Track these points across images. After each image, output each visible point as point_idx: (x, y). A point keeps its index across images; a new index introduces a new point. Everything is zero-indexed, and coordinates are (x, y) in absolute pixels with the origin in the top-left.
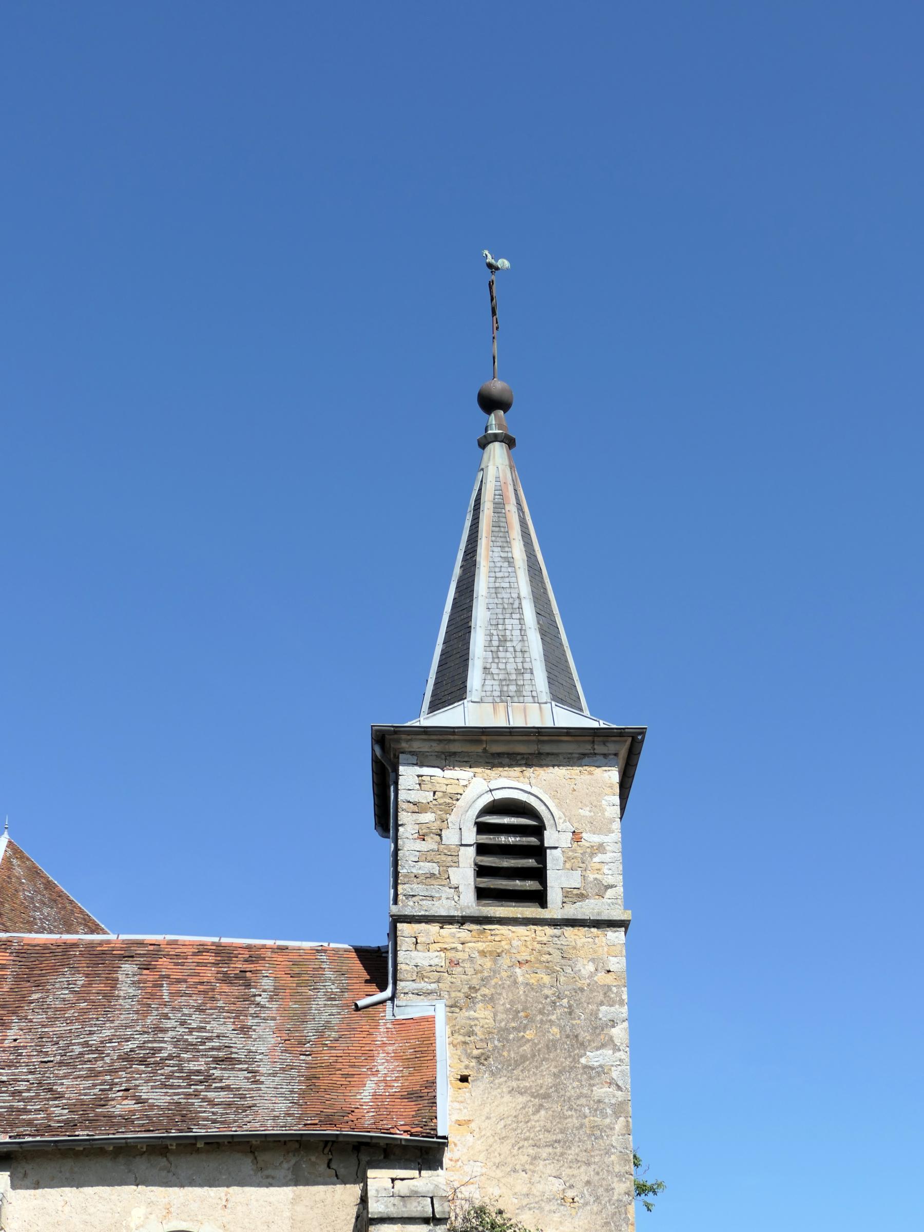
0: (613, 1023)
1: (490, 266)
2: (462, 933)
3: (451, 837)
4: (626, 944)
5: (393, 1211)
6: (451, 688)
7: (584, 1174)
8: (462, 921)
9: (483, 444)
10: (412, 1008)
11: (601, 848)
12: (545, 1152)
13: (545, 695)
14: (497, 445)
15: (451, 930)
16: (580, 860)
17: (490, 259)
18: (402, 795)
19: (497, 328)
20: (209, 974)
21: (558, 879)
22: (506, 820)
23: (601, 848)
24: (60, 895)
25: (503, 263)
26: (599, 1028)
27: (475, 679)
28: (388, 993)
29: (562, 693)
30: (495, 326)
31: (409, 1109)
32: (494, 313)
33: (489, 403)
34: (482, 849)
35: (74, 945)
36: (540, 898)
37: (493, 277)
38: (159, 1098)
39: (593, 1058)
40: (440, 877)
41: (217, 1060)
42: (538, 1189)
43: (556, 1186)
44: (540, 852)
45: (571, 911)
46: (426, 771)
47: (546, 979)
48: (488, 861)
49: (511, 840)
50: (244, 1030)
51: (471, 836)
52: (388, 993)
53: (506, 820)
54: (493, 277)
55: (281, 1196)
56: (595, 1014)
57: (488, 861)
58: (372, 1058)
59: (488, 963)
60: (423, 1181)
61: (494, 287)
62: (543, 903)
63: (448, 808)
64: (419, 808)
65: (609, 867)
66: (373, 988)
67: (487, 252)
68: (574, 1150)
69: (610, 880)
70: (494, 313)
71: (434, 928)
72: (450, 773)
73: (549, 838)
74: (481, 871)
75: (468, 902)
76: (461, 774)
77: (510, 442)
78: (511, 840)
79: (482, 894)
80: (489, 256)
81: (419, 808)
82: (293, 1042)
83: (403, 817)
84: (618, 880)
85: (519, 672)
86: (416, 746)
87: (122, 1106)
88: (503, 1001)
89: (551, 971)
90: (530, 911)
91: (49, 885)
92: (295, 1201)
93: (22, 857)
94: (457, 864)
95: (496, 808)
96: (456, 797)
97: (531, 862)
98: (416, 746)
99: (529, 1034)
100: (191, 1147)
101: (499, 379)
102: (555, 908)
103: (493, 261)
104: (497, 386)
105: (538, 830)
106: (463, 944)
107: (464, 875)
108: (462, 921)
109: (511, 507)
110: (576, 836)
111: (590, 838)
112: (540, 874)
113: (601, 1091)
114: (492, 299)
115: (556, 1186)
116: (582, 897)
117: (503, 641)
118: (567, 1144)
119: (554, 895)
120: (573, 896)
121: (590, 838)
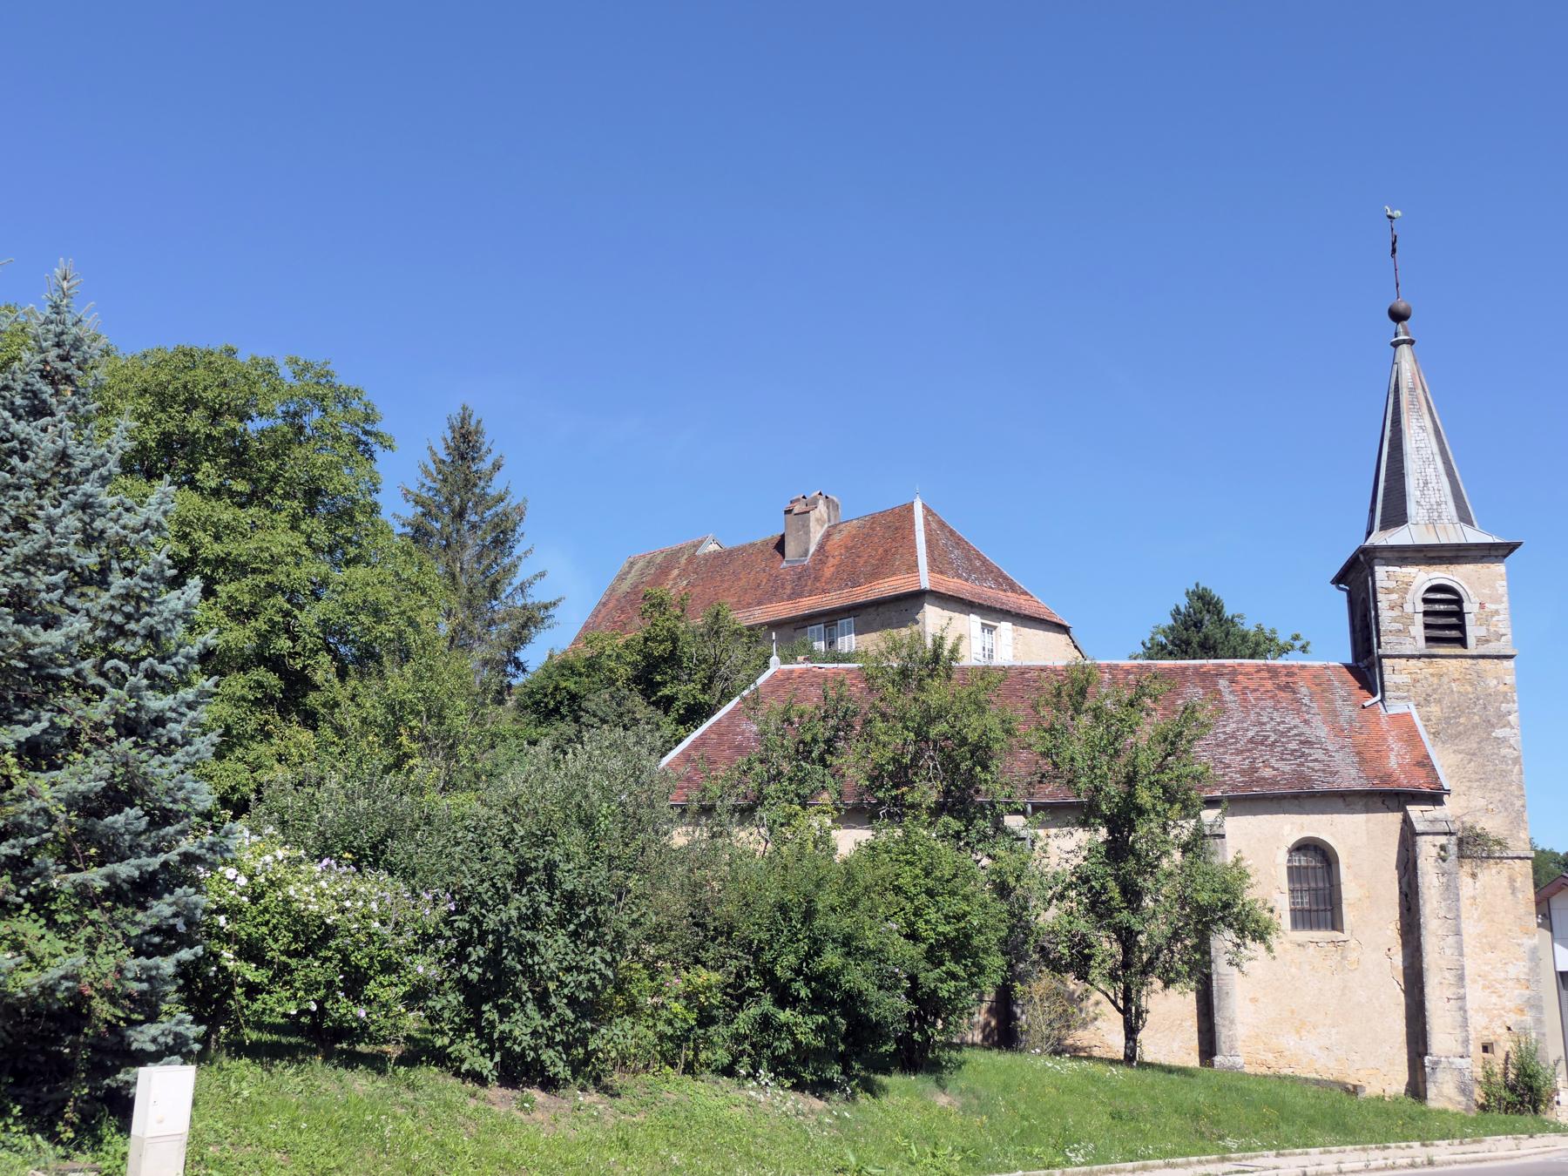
0: (1509, 713)
2: (1420, 663)
3: (1408, 608)
4: (1516, 668)
5: (1428, 829)
6: (1395, 514)
7: (1498, 796)
8: (1419, 657)
9: (1396, 345)
10: (1396, 708)
11: (1497, 612)
12: (1475, 785)
13: (1456, 519)
14: (1405, 346)
15: (1412, 662)
16: (1485, 620)
18: (1378, 584)
20: (1269, 685)
21: (1473, 631)
22: (1439, 596)
23: (1497, 612)
24: (960, 539)
25: (1397, 213)
26: (1502, 717)
27: (1412, 508)
28: (1379, 697)
29: (1465, 517)
31: (1421, 772)
32: (1394, 251)
33: (1398, 316)
34: (1426, 614)
35: (1186, 668)
36: (1462, 642)
38: (1286, 767)
39: (1499, 733)
40: (1404, 632)
41: (1302, 742)
42: (1472, 804)
43: (1483, 802)
44: (1460, 614)
45: (1482, 650)
46: (1391, 568)
47: (1470, 689)
48: (1431, 620)
49: (1442, 607)
50: (1306, 722)
51: (1421, 607)
52: (1379, 697)
53: (1439, 596)
55: (1361, 818)
56: (1499, 708)
57: (1431, 620)
58: (1385, 740)
59: (1435, 680)
60: (1435, 812)
62: (1464, 645)
63: (1406, 591)
64: (1389, 591)
65: (1502, 623)
66: (1365, 693)
68: (1491, 784)
69: (1503, 631)
70: (1394, 251)
71: (1404, 661)
72: (1404, 570)
73: (1467, 607)
74: (1427, 626)
75: (1421, 646)
76: (1411, 570)
77: (1411, 342)
78: (1442, 607)
79: (1428, 639)
81: (1389, 591)
82: (1338, 732)
83: (1380, 596)
84: (1508, 631)
85: (1438, 504)
86: (1385, 554)
87: (1267, 773)
88: (1446, 702)
89: (1472, 685)
90: (1459, 651)
91: (952, 532)
92: (1368, 821)
93: (933, 515)
94: (1413, 624)
95: (1432, 589)
96: (1409, 584)
97: (1454, 620)
98: (1385, 554)
99: (1462, 720)
100: (1313, 795)
102: (1473, 647)
104: (1401, 306)
105: (1459, 602)
107: (1418, 631)
108: (1419, 657)
109: (1420, 391)
110: (1482, 605)
111: (1490, 607)
112: (1461, 627)
113: (1504, 751)
115: (1483, 802)
116: (1488, 641)
117: (1426, 483)
118: (1488, 780)
119: (1471, 640)
120: (1482, 641)
121: (1490, 607)
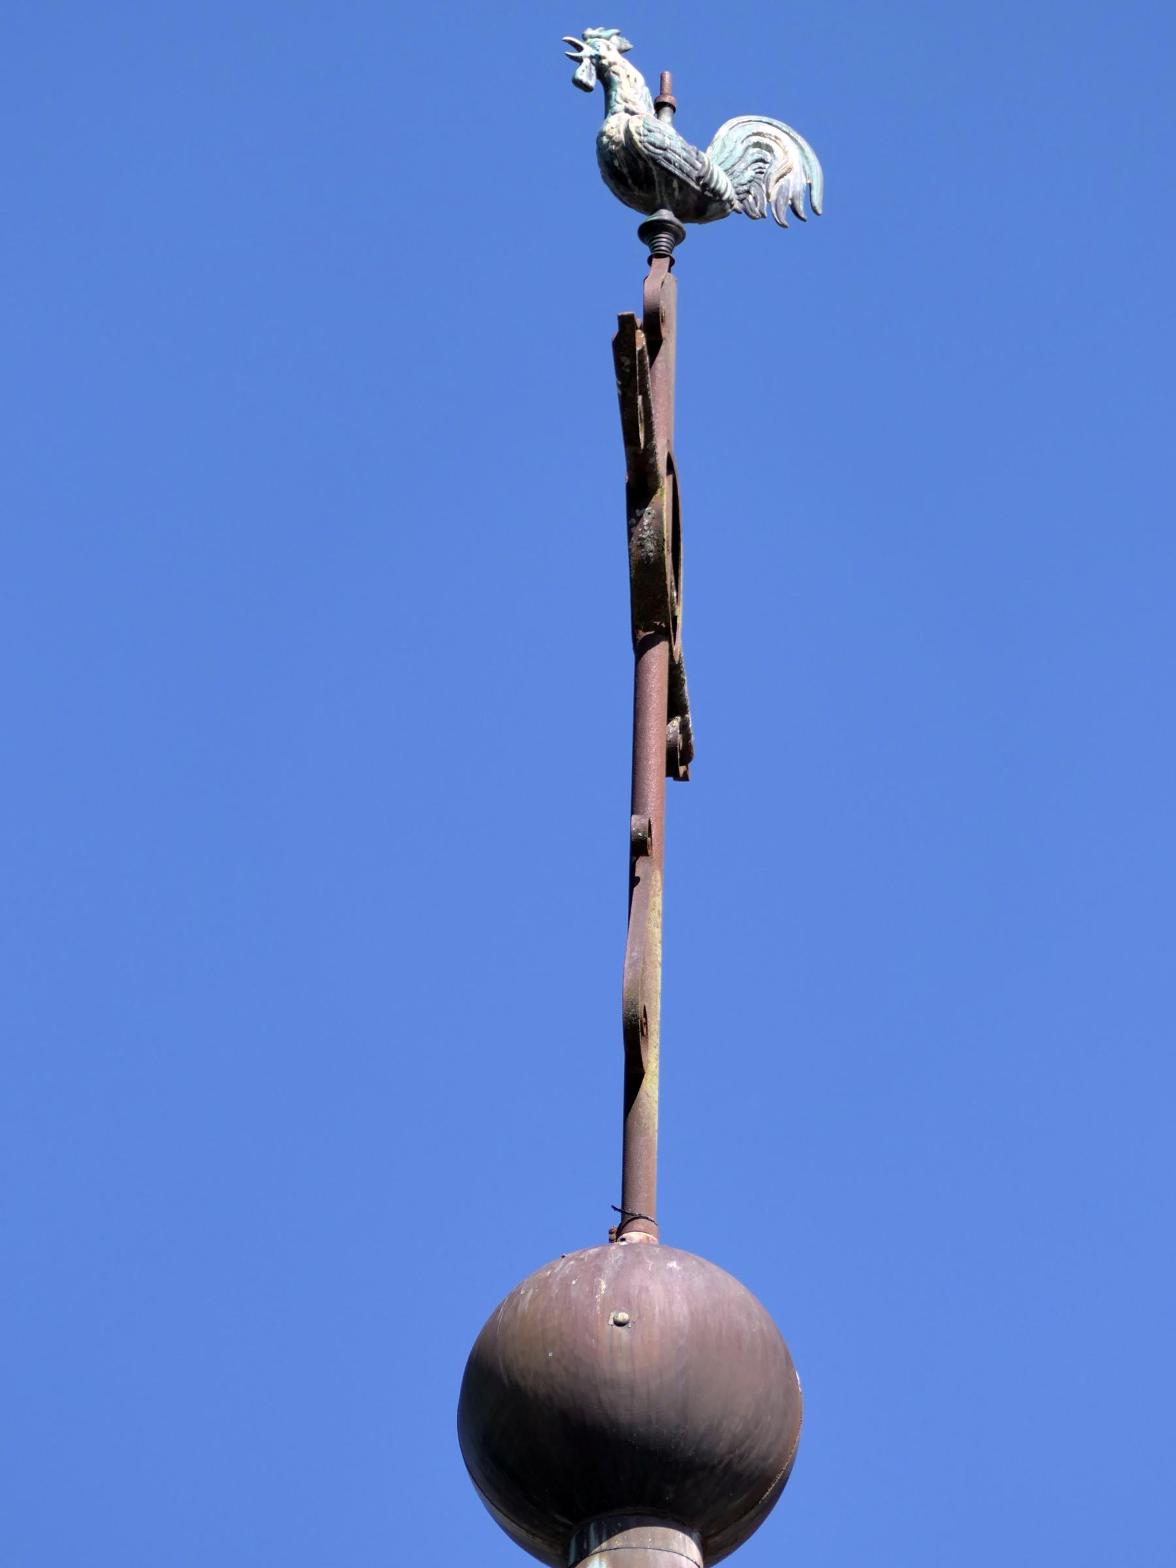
1: (634, 173)
17: (634, 113)
19: (678, 759)
25: (759, 156)
30: (660, 731)
32: (651, 614)
37: (660, 284)
54: (660, 284)
61: (664, 375)
67: (606, 44)
70: (651, 614)
77: (674, 109)
80: (632, 87)
100: (636, 676)
101: (674, 1239)
103: (663, 134)
104: (653, 1306)
106: (627, 1218)
114: (640, 489)
